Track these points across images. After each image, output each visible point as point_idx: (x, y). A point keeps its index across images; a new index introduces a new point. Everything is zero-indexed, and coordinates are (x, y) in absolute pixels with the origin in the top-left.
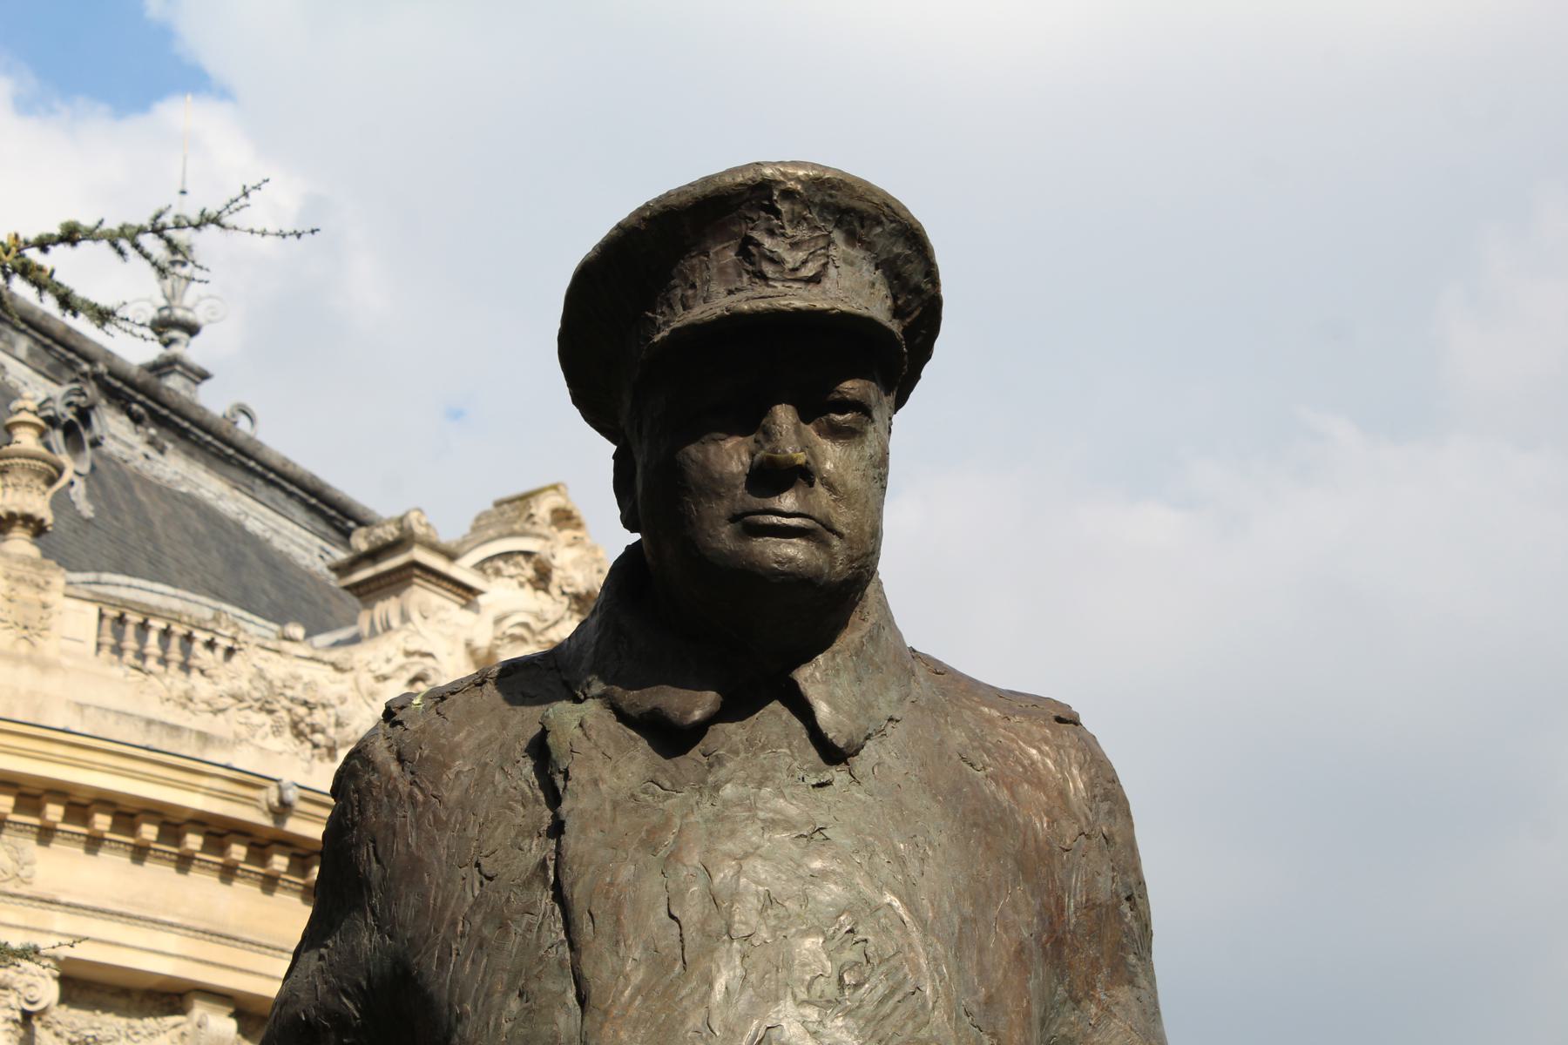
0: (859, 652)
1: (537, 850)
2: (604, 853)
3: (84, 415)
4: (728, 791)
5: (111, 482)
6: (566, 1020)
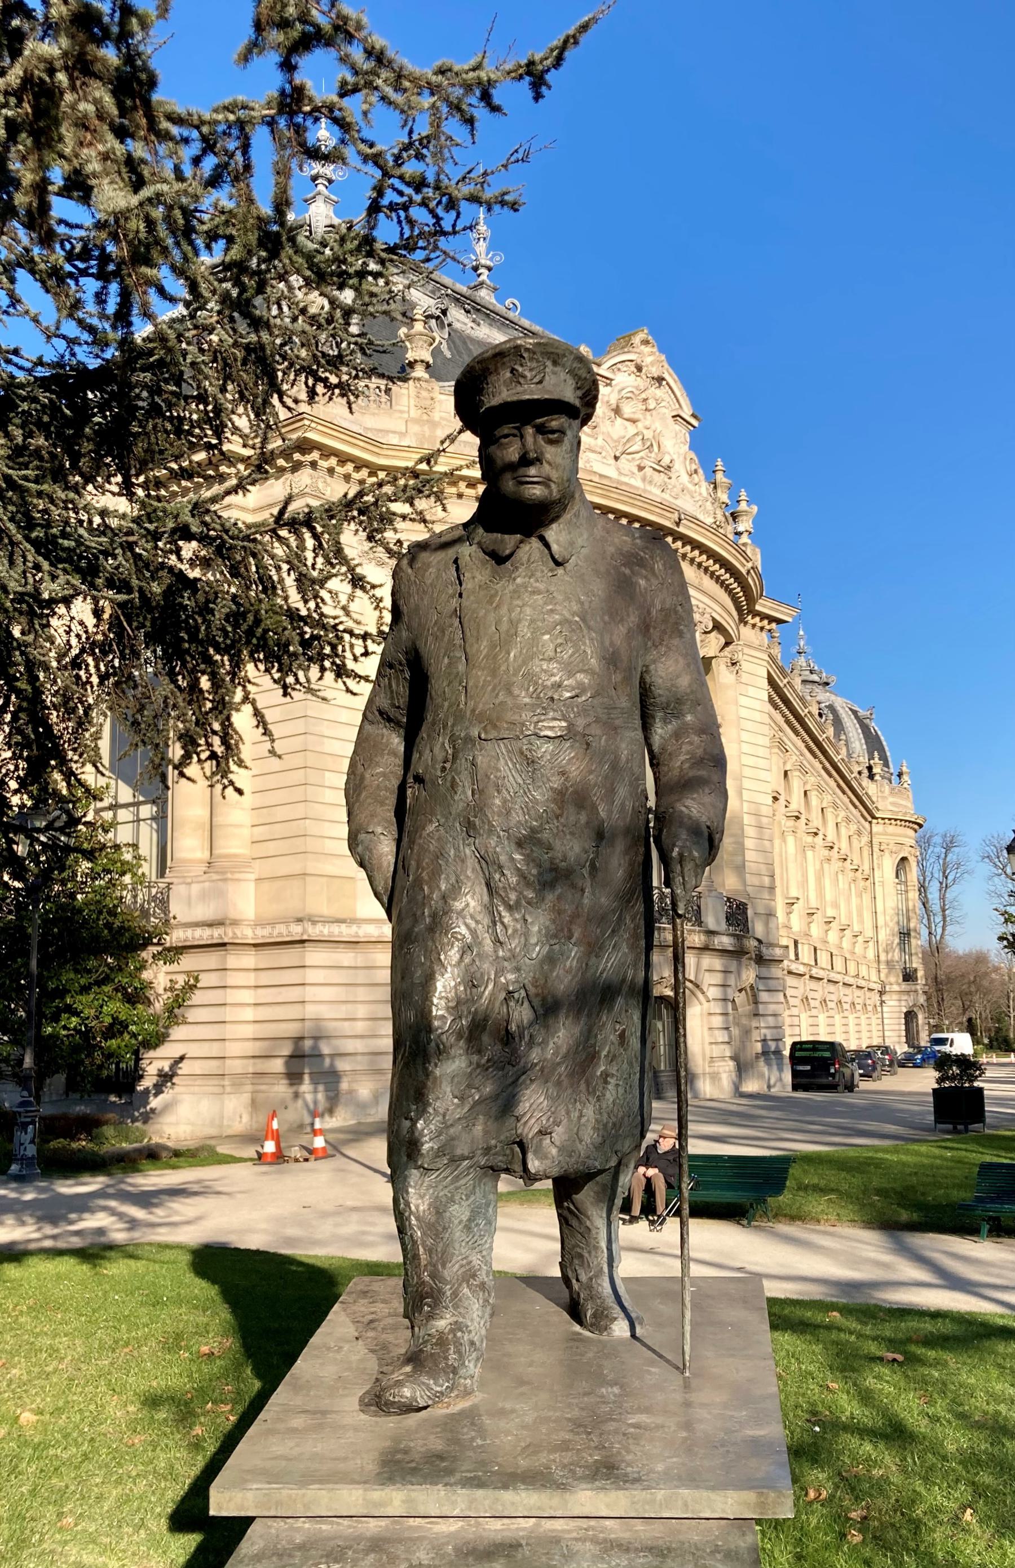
0: (570, 522)
1: (454, 602)
2: (475, 606)
3: (444, 312)
4: (519, 580)
5: (457, 341)
6: (461, 667)
